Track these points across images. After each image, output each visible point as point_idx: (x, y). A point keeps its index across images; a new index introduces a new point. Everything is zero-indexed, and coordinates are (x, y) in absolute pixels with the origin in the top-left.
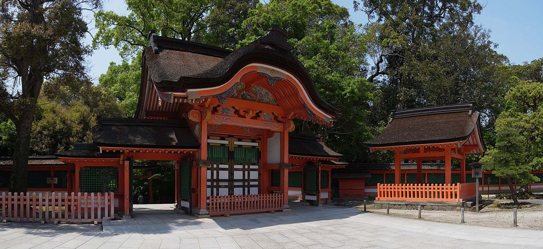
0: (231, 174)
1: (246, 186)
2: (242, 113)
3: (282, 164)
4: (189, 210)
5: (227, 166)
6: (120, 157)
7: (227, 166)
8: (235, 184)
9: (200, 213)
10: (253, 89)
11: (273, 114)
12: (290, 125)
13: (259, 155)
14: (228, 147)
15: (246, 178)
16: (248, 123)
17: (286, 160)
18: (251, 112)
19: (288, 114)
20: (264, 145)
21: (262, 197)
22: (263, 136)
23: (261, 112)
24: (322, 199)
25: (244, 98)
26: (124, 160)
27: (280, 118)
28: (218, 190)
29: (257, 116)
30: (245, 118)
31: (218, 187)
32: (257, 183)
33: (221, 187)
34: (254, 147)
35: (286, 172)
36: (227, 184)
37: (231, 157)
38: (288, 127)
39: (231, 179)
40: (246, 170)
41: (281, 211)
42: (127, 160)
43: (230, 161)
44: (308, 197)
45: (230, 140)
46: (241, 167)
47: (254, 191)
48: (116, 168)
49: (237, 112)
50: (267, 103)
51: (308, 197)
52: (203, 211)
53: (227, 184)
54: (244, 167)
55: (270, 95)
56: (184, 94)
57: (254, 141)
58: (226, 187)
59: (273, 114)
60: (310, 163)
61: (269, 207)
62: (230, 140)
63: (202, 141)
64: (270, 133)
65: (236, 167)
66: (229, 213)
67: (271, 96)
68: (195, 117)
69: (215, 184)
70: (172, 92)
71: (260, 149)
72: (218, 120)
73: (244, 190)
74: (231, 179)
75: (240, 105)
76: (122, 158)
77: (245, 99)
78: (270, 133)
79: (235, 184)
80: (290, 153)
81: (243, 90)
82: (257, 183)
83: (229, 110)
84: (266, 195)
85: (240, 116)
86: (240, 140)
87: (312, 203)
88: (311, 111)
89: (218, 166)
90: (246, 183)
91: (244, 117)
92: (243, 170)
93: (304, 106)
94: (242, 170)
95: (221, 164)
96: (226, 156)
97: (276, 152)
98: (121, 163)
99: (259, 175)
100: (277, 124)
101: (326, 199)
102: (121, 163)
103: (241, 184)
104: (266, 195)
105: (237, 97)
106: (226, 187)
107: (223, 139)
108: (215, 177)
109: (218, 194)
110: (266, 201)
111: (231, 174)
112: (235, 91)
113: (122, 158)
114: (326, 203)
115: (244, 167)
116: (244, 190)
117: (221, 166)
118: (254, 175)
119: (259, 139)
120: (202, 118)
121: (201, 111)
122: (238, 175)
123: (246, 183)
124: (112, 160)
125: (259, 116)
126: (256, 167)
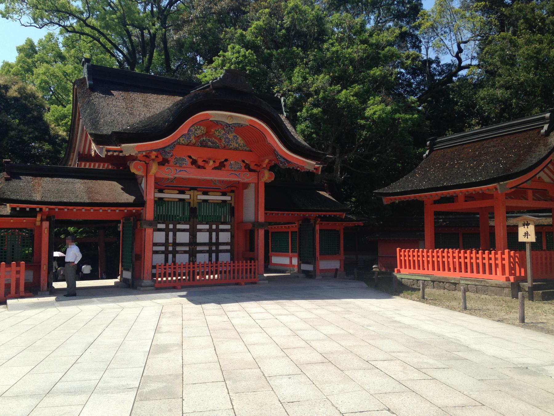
0: (193, 236)
1: (214, 251)
2: (200, 163)
3: (256, 224)
4: (131, 281)
5: (187, 227)
6: (36, 217)
7: (187, 227)
8: (199, 248)
9: (143, 284)
10: (217, 133)
11: (243, 161)
12: (264, 175)
13: (233, 211)
14: (190, 203)
15: (214, 240)
16: (208, 175)
17: (261, 219)
18: (211, 163)
19: (263, 161)
20: (239, 199)
21: (241, 264)
22: (235, 189)
23: (226, 160)
24: (322, 271)
25: (204, 145)
26: (42, 220)
27: (252, 167)
28: (174, 257)
29: (221, 166)
30: (205, 168)
31: (218, 252)
32: (228, 247)
33: (178, 252)
34: (224, 202)
35: (261, 233)
36: (187, 248)
37: (193, 215)
38: (263, 177)
39: (193, 242)
40: (214, 230)
41: (255, 283)
42: (47, 220)
43: (192, 220)
44: (305, 267)
45: (192, 194)
46: (207, 227)
47: (225, 258)
48: (31, 230)
49: (194, 162)
50: (236, 149)
51: (305, 267)
52: (147, 282)
53: (187, 248)
54: (211, 227)
55: (240, 139)
56: (119, 147)
57: (224, 194)
58: (185, 252)
59: (243, 161)
60: (306, 220)
61: (238, 278)
62: (192, 194)
63: (148, 198)
64: (246, 185)
65: (199, 227)
66: (199, 285)
67: (240, 141)
68: (139, 170)
69: (170, 248)
70: (103, 145)
71: (233, 205)
72: (168, 173)
73: (210, 256)
74: (193, 242)
75: (198, 154)
76: (39, 218)
77: (205, 146)
78: (246, 185)
79: (199, 248)
80: (266, 209)
81: (202, 136)
82: (228, 247)
83: (183, 159)
84: (242, 262)
85: (199, 167)
86: (205, 193)
87: (309, 275)
88: (284, 158)
89: (175, 226)
90: (214, 247)
91: (204, 168)
92: (210, 231)
93: (273, 152)
94: (208, 230)
95: (179, 223)
96: (187, 213)
97: (252, 208)
98: (38, 223)
99: (232, 236)
100: (248, 174)
101: (337, 270)
102: (38, 223)
103: (207, 248)
104: (242, 262)
105: (194, 145)
106: (185, 252)
107: (182, 192)
108: (214, 240)
109: (174, 262)
110: (242, 269)
111: (193, 236)
112: (192, 137)
113: (39, 218)
114: (335, 276)
115: (211, 227)
116: (210, 256)
117: (179, 226)
118: (225, 237)
119: (232, 191)
120: (147, 171)
121: (147, 162)
122: (203, 237)
123: (214, 247)
124: (25, 220)
125: (224, 166)
126: (228, 227)
